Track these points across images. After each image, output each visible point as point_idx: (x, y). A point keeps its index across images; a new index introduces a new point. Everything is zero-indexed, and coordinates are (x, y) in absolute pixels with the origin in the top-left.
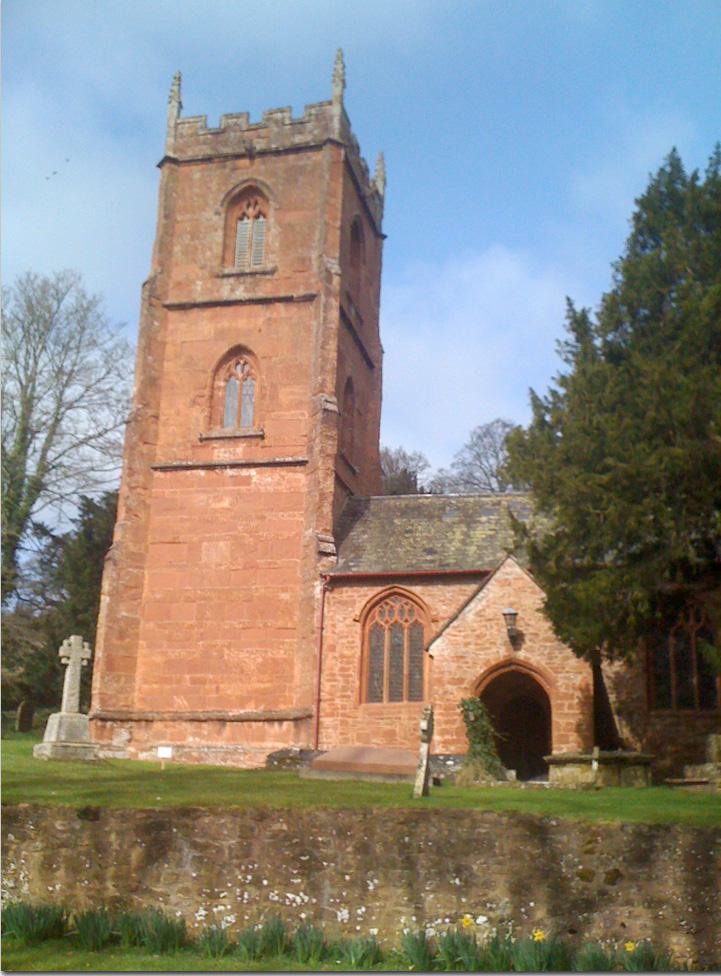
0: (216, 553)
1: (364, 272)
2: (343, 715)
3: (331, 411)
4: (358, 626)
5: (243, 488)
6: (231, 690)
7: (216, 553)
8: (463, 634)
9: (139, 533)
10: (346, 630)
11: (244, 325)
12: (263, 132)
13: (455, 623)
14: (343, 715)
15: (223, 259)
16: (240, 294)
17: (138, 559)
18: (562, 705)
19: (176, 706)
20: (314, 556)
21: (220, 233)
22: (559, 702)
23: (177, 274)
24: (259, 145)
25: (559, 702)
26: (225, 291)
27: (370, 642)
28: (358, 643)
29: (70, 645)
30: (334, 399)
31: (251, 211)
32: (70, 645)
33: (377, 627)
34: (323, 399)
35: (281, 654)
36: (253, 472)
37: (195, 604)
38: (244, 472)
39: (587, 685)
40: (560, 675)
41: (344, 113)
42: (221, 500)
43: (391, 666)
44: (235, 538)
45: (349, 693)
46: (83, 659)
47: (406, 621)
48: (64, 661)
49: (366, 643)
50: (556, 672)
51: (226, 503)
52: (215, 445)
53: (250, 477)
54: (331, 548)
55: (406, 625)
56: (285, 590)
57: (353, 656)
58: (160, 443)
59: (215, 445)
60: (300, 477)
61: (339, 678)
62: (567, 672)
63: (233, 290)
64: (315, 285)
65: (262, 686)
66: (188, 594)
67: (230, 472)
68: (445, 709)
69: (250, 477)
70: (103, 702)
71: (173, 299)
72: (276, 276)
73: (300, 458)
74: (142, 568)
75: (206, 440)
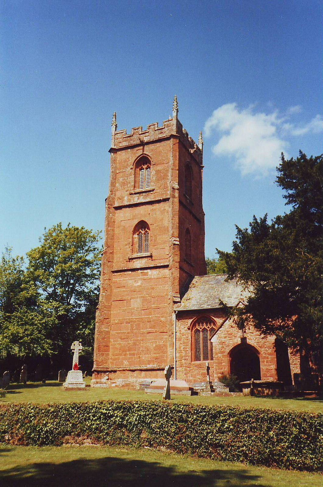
0: (136, 303)
1: (193, 183)
2: (185, 367)
3: (176, 244)
4: (190, 331)
5: (145, 277)
6: (145, 357)
7: (136, 303)
8: (223, 333)
9: (108, 298)
10: (185, 332)
11: (141, 213)
12: (147, 134)
13: (220, 329)
14: (185, 367)
15: (135, 187)
16: (142, 200)
17: (109, 308)
18: (264, 361)
19: (124, 365)
20: (172, 303)
21: (133, 176)
22: (263, 360)
23: (118, 194)
24: (146, 139)
25: (263, 360)
26: (136, 200)
27: (195, 336)
28: (190, 337)
29: (74, 345)
30: (178, 239)
31: (145, 167)
32: (74, 345)
33: (197, 331)
34: (173, 240)
35: (162, 343)
36: (149, 271)
37: (130, 324)
38: (145, 271)
39: (259, 355)
40: (263, 349)
41: (178, 122)
42: (138, 282)
43: (204, 346)
44: (143, 297)
45: (187, 358)
46: (79, 350)
47: (201, 328)
48: (73, 351)
49: (193, 337)
50: (261, 348)
51: (139, 284)
52: (134, 261)
53: (147, 273)
54: (179, 300)
55: (201, 330)
56: (162, 317)
57: (188, 343)
58: (115, 261)
59: (134, 261)
60: (166, 271)
61: (184, 352)
62: (265, 348)
63: (138, 199)
64: (168, 194)
65: (155, 355)
66: (127, 320)
67: (140, 271)
68: (218, 364)
69: (147, 273)
70: (97, 365)
71: (116, 205)
72: (154, 192)
73: (166, 264)
74: (110, 311)
75: (131, 259)
